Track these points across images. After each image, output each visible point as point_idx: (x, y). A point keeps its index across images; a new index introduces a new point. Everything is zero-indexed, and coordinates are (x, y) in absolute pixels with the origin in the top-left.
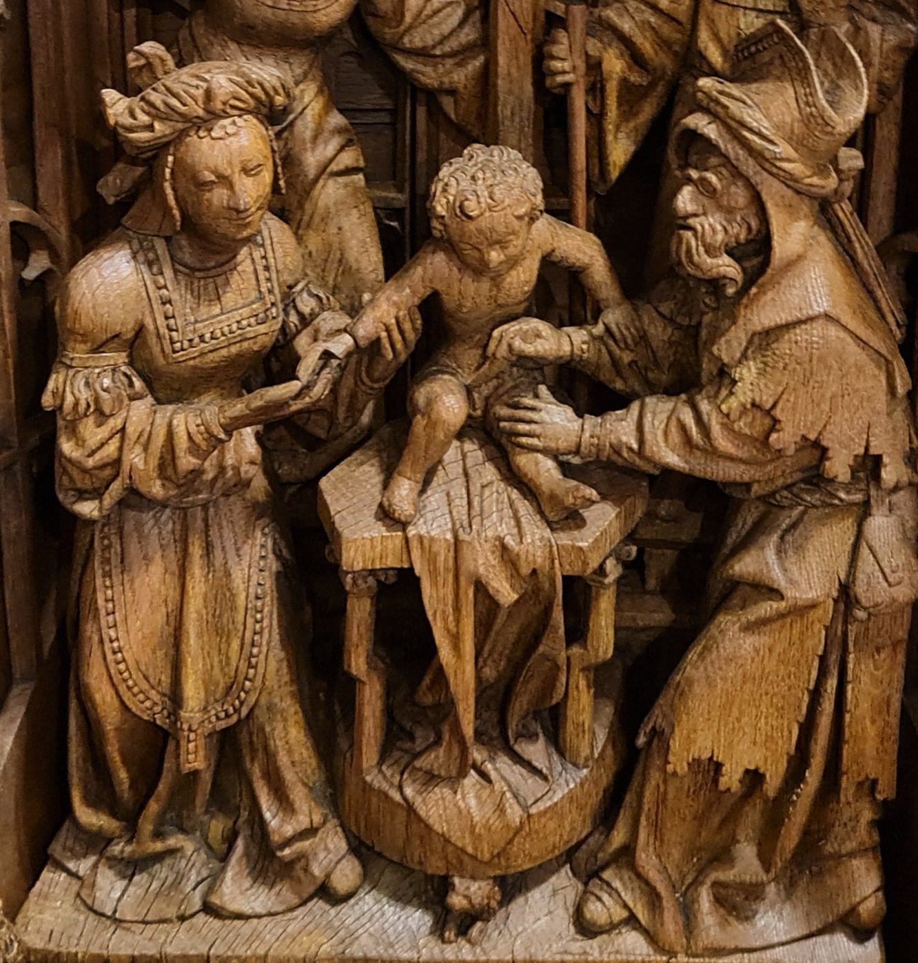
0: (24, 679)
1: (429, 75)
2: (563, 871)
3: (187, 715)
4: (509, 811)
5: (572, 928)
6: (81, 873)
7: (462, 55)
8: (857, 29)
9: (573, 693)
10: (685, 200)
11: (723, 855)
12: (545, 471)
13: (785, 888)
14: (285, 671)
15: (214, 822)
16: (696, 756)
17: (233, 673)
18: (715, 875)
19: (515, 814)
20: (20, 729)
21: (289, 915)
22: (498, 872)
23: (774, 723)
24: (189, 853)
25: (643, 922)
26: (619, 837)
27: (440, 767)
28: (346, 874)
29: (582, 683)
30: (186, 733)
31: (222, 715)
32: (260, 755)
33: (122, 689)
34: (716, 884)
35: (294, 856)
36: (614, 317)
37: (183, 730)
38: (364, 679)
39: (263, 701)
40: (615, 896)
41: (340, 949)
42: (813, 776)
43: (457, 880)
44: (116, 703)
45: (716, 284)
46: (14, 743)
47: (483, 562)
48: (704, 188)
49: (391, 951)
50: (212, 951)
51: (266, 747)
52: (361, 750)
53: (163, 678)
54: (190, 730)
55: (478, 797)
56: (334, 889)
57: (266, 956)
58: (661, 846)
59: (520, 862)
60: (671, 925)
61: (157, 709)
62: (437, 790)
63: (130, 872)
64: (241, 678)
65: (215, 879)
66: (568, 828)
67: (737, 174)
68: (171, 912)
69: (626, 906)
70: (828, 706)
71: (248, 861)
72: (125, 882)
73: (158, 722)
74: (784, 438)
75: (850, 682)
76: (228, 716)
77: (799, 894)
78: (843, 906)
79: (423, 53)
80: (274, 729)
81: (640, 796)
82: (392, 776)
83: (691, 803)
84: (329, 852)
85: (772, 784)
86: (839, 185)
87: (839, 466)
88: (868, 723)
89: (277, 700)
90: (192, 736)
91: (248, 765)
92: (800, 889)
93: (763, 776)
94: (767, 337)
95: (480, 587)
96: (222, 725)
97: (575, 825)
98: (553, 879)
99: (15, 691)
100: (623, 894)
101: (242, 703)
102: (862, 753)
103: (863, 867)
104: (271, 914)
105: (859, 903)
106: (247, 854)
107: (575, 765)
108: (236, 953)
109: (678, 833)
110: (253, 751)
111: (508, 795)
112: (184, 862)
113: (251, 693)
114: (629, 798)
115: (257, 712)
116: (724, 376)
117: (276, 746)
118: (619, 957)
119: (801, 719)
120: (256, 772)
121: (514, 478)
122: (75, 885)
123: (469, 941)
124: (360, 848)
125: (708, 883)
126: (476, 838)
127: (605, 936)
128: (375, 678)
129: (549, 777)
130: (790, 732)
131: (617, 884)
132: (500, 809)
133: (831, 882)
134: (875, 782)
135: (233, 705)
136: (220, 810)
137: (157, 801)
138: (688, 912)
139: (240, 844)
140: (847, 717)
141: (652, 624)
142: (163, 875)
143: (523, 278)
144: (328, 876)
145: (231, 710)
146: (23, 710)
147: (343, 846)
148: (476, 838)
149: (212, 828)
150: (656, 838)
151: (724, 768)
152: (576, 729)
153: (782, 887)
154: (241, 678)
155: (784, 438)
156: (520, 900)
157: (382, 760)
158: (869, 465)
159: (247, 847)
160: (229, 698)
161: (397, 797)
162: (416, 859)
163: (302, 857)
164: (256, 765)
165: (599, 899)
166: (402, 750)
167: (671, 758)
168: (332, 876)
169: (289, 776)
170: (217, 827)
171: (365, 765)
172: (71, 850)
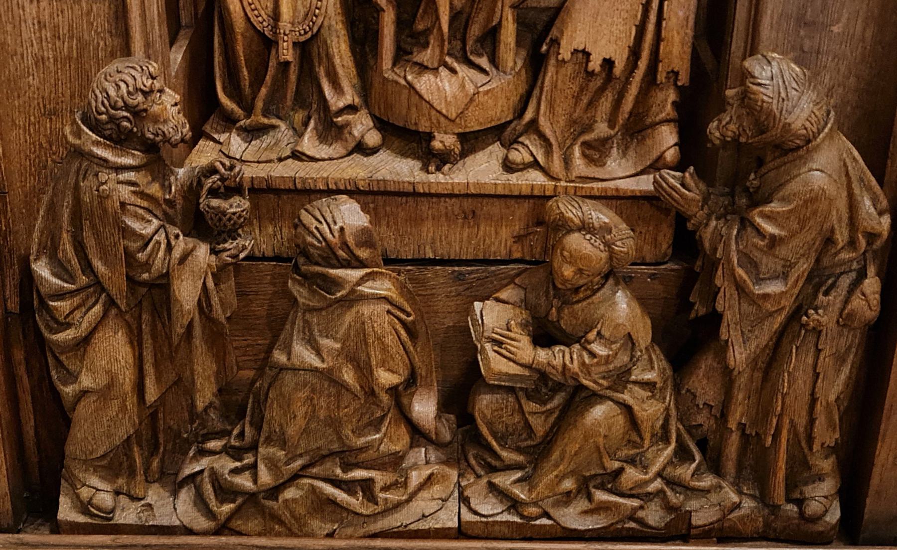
0: (187, 27)
2: (496, 144)
3: (283, 24)
4: (467, 86)
5: (501, 169)
6: (221, 141)
9: (504, 23)
11: (588, 128)
13: (623, 151)
14: (339, 6)
15: (296, 115)
16: (576, 48)
17: (308, 5)
18: (581, 139)
19: (471, 89)
20: (185, 51)
21: (340, 160)
22: (460, 130)
23: (622, 28)
24: (283, 130)
25: (541, 163)
26: (529, 115)
27: (427, 61)
28: (373, 138)
29: (510, 18)
30: (282, 35)
31: (302, 32)
32: (324, 60)
33: (248, 10)
34: (584, 144)
35: (344, 123)
37: (280, 33)
38: (385, 8)
39: (326, 24)
40: (526, 149)
41: (370, 175)
42: (643, 64)
43: (436, 134)
44: (242, 14)
46: (182, 59)
49: (398, 177)
50: (297, 175)
51: (327, 55)
52: (382, 58)
53: (269, 5)
54: (285, 34)
55: (449, 81)
56: (366, 144)
57: (328, 177)
58: (553, 117)
59: (472, 124)
60: (557, 165)
61: (265, 24)
62: (426, 75)
63: (249, 140)
64: (313, 7)
66: (500, 109)
68: (274, 156)
69: (532, 154)
70: (653, 17)
71: (317, 132)
72: (247, 145)
73: (266, 33)
75: (665, 19)
76: (306, 33)
77: (630, 153)
78: (655, 154)
80: (332, 41)
81: (543, 83)
82: (400, 72)
83: (571, 86)
84: (363, 125)
88: (675, 33)
89: (334, 23)
90: (286, 38)
91: (317, 70)
92: (632, 149)
93: (613, 62)
96: (302, 39)
98: (490, 147)
99: (182, 32)
100: (530, 147)
101: (314, 23)
102: (671, 52)
103: (668, 131)
104: (331, 159)
105: (665, 151)
106: (315, 128)
107: (505, 73)
108: (311, 176)
109: (563, 108)
110: (320, 58)
111: (467, 78)
112: (280, 134)
113: (319, 17)
114: (536, 92)
115: (322, 31)
117: (333, 52)
118: (528, 182)
119: (637, 23)
120: (322, 72)
122: (218, 147)
123: (443, 173)
124: (381, 124)
125: (579, 143)
126: (448, 104)
127: (520, 173)
128: (391, 9)
129: (490, 73)
130: (631, 33)
131: (527, 142)
132: (463, 86)
133: (649, 142)
134: (677, 74)
135: (308, 26)
136: (300, 107)
137: (265, 88)
138: (567, 162)
139: (312, 124)
140: (664, 23)
141: (551, 6)
142: (268, 141)
144: (362, 137)
145: (308, 28)
146: (187, 42)
147: (371, 124)
148: (448, 104)
149: (296, 118)
150: (550, 112)
151: (591, 57)
152: (506, 48)
153: (620, 151)
154: (313, 7)
156: (471, 157)
157: (394, 65)
159: (316, 124)
160: (306, 22)
161: (403, 82)
162: (413, 121)
163: (348, 124)
164: (322, 68)
165: (517, 150)
166: (406, 60)
167: (561, 51)
168: (365, 137)
169: (340, 71)
171: (384, 68)
172: (216, 129)
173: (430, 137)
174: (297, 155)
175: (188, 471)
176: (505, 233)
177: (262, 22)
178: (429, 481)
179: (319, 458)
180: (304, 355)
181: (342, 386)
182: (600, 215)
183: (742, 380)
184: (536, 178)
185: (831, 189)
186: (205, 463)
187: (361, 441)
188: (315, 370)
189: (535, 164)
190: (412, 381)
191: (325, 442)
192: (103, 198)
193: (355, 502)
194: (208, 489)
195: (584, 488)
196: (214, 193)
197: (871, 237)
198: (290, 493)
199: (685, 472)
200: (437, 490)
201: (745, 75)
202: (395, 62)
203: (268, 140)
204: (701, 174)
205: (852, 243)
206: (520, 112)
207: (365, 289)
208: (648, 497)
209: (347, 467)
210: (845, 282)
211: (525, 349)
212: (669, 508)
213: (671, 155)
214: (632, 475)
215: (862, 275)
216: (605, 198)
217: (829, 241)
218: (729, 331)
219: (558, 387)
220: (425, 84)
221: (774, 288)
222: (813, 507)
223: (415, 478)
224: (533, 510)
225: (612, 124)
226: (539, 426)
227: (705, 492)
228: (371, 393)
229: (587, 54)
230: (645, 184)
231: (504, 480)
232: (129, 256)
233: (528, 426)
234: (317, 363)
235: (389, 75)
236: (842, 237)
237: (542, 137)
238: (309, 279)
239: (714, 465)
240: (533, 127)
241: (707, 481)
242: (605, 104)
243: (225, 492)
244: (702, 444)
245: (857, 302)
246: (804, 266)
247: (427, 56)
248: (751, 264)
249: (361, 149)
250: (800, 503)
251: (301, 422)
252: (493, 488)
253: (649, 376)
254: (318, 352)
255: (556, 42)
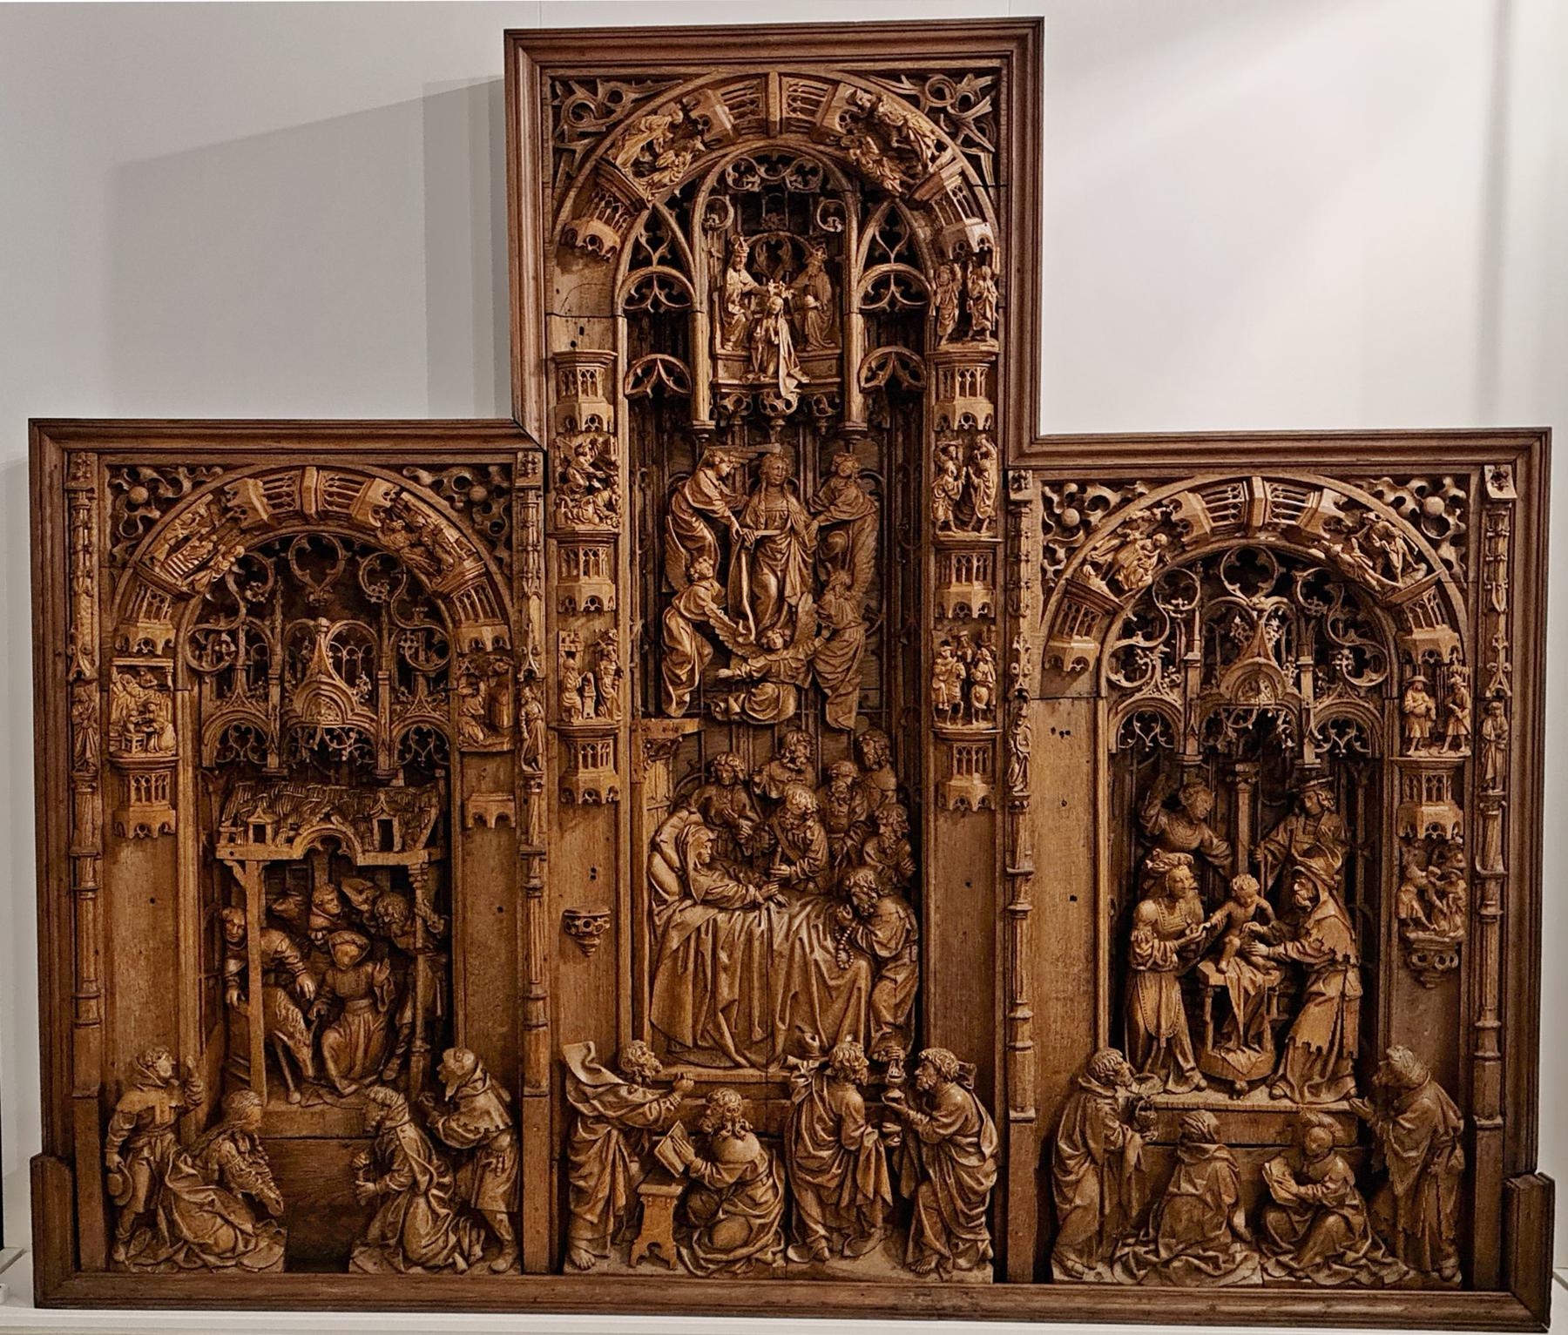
1: (1217, 862)
7: (1227, 857)
8: (717, 1131)
10: (1296, 887)
11: (1310, 1079)
12: (1260, 961)
26: (1281, 1072)
28: (1203, 1083)
36: (1273, 923)
42: (1336, 1049)
45: (1305, 908)
47: (1246, 983)
48: (1301, 884)
60: (1297, 1097)
65: (1166, 1082)
67: (1309, 879)
74: (1325, 948)
79: (1216, 857)
85: (1325, 1052)
86: (916, 1190)
87: (1339, 957)
94: (1319, 922)
95: (1246, 991)
97: (1265, 1070)
109: (1297, 1069)
116: (1308, 933)
121: (1249, 963)
124: (1205, 1076)
143: (1252, 909)
155: (1325, 948)
158: (1347, 957)
170: (1163, 1072)
173: (1233, 1083)
174: (1166, 1091)
175: (1118, 1254)
176: (1272, 1130)
177: (1152, 1029)
178: (1246, 1258)
179: (1190, 1246)
180: (1186, 1187)
181: (1206, 1203)
182: (1327, 1120)
183: (1402, 1204)
184: (1286, 1103)
185: (1433, 1107)
186: (1127, 1250)
187: (1213, 1235)
188: (1192, 1195)
189: (1286, 1096)
190: (1235, 1206)
191: (1194, 1236)
192: (1098, 1110)
193: (1209, 1269)
194: (1132, 1263)
195: (1326, 1264)
196: (1142, 1109)
197: (1455, 1129)
198: (1176, 1264)
199: (1379, 1255)
200: (1250, 1264)
201: (1388, 1057)
202: (1214, 1046)
203: (1149, 1084)
204: (1372, 1100)
205: (1447, 1133)
206: (1275, 1070)
207: (1217, 1154)
208: (1361, 1267)
209: (1205, 1250)
210: (1447, 1152)
211: (1294, 1188)
212: (1373, 1274)
213: (1353, 1092)
214: (1351, 1255)
215: (1454, 1148)
216: (1329, 1113)
217: (1435, 1131)
218: (1394, 1177)
219: (1311, 1206)
220: (1230, 1057)
221: (1413, 1154)
222: (1448, 1272)
223: (1239, 1257)
224: (1300, 1274)
225: (1322, 1075)
226: (1301, 1230)
227: (1390, 1265)
228: (1219, 1207)
229: (1309, 1045)
230: (1345, 1105)
231: (1285, 1259)
232: (1107, 1137)
233: (1294, 1229)
234: (1193, 1191)
235: (1215, 1053)
236: (1441, 1130)
237: (1288, 1082)
238: (1188, 1150)
239: (1392, 1252)
240: (1284, 1077)
241: (1389, 1260)
242: (1318, 1067)
243: (1141, 1263)
244: (1385, 1241)
245: (1453, 1161)
246: (1426, 1143)
247: (1231, 1045)
248: (1402, 1144)
249: (1198, 1088)
250: (1439, 1270)
251: (1184, 1223)
252: (1279, 1263)
253: (1355, 1202)
254: (1195, 1187)
255: (1293, 1039)
